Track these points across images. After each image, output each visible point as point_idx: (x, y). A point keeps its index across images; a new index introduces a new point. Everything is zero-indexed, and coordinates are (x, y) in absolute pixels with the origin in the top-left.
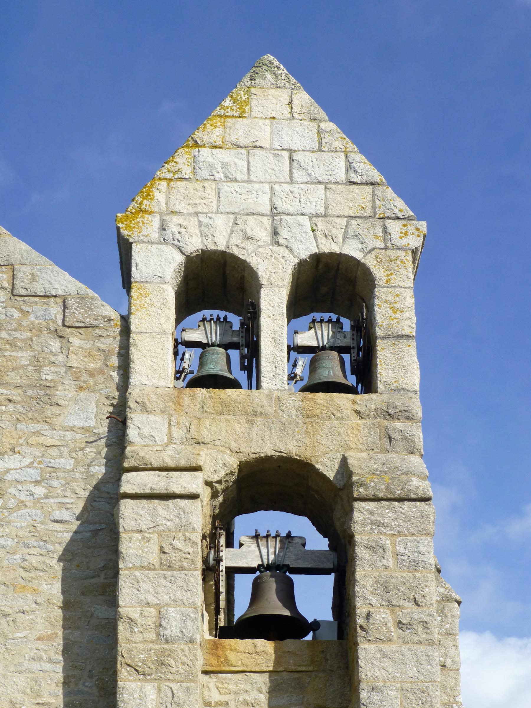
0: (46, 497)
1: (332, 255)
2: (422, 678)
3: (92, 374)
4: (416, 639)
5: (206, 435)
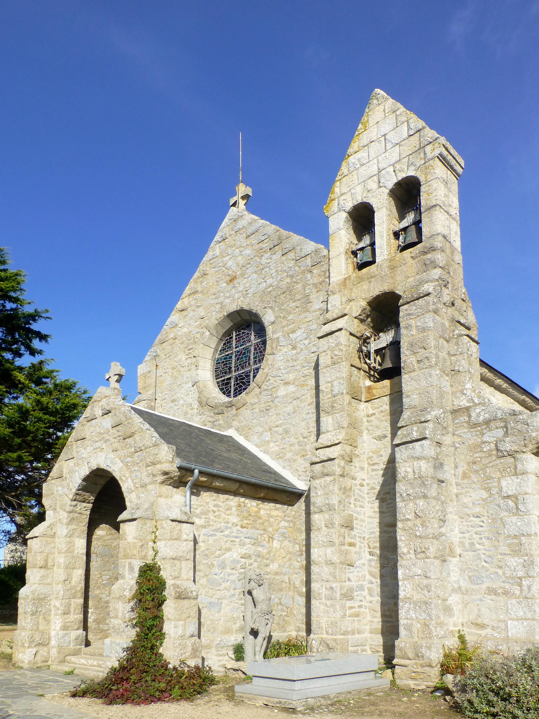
0: (309, 344)
1: (403, 179)
2: (427, 385)
3: (321, 284)
4: (425, 366)
5: (353, 296)
